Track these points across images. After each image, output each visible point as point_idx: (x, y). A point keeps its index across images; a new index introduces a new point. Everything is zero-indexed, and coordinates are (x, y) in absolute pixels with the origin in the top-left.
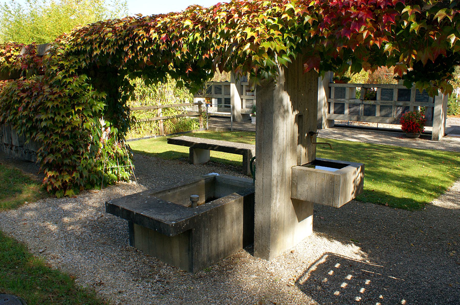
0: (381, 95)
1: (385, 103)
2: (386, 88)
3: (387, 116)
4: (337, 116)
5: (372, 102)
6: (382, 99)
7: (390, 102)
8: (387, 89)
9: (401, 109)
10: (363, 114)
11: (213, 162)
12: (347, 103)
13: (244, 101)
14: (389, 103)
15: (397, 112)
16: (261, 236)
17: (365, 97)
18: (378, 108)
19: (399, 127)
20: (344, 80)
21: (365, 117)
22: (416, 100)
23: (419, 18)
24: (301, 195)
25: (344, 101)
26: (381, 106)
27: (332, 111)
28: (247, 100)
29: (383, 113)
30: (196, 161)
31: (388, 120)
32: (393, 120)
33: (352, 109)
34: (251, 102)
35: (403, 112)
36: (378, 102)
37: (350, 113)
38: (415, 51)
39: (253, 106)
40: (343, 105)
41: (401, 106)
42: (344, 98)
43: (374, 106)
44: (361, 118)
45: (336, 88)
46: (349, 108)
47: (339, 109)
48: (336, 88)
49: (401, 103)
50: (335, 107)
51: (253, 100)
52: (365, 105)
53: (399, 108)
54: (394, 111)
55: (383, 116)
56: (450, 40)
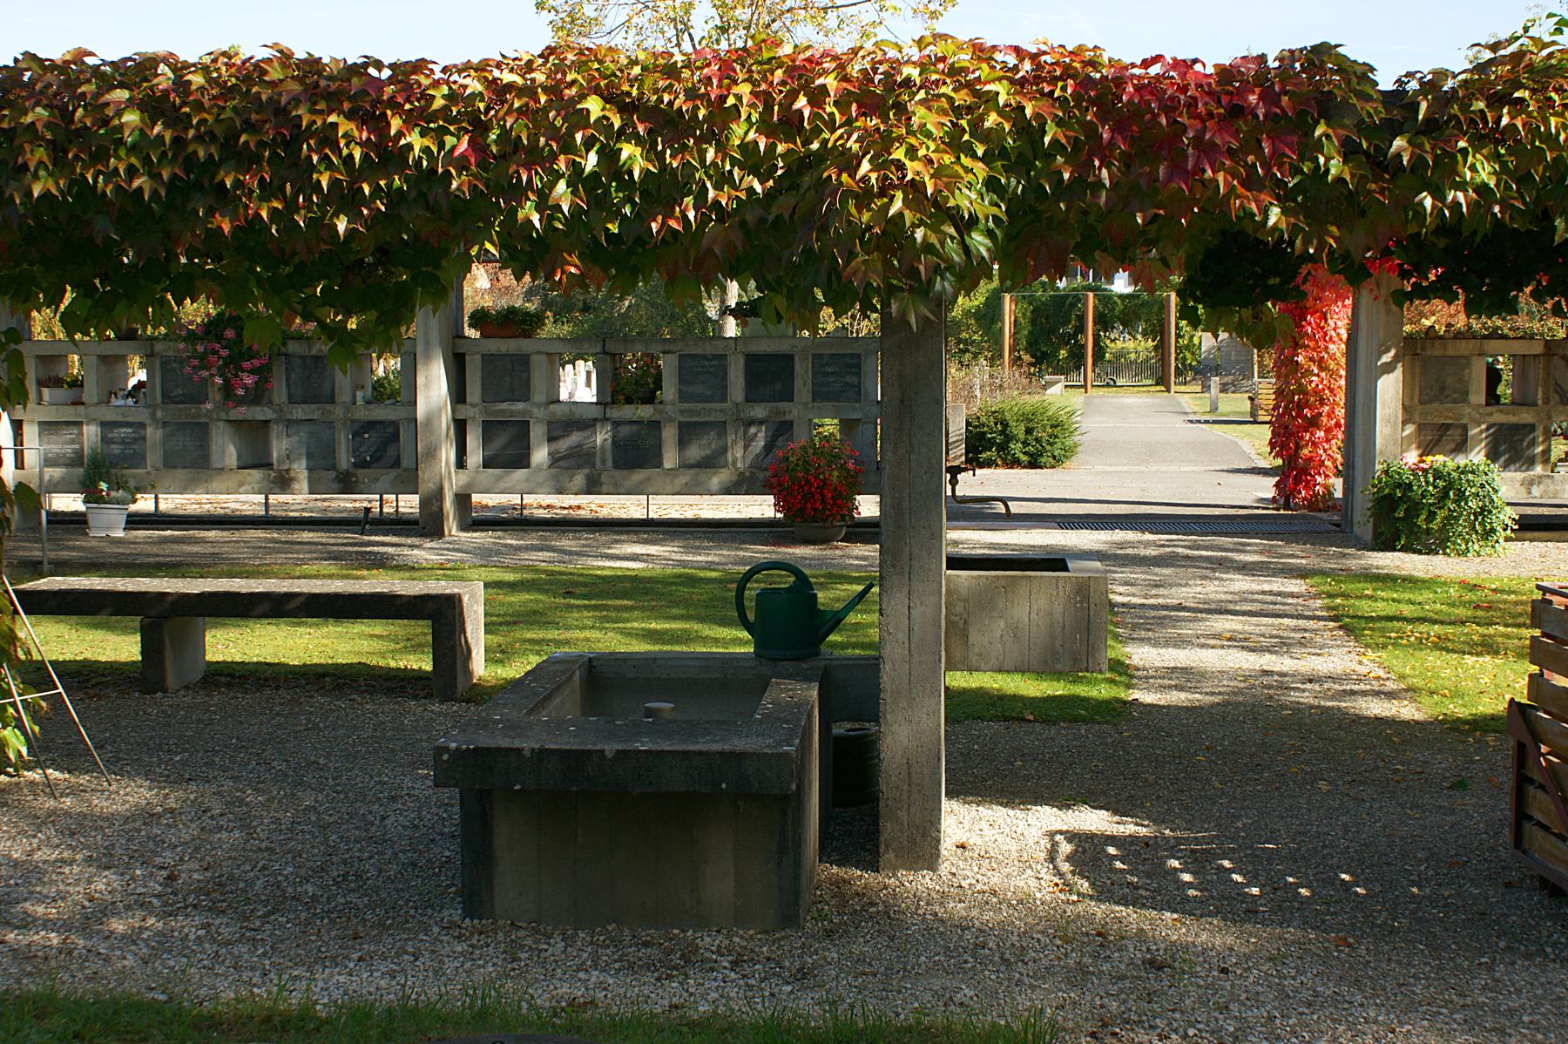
0: (681, 381)
1: (699, 413)
2: (699, 352)
3: (710, 463)
4: (499, 479)
5: (645, 412)
6: (683, 397)
7: (717, 406)
8: (704, 357)
9: (761, 435)
10: (610, 463)
11: (232, 676)
12: (539, 420)
13: (31, 433)
14: (713, 411)
15: (746, 448)
16: (905, 797)
17: (614, 393)
18: (669, 434)
19: (762, 507)
20: (524, 322)
21: (618, 473)
22: (816, 396)
23: (1349, 151)
24: (980, 655)
25: (525, 412)
26: (681, 425)
27: (475, 457)
28: (47, 427)
29: (695, 452)
30: (171, 680)
31: (715, 482)
32: (734, 478)
33: (564, 444)
34: (70, 434)
35: (768, 448)
36: (668, 408)
37: (555, 459)
38: (1333, 229)
39: (79, 454)
40: (524, 427)
41: (761, 422)
42: (526, 398)
43: (655, 426)
44: (604, 478)
45: (488, 359)
46: (551, 440)
47: (505, 448)
48: (488, 359)
49: (759, 411)
50: (486, 440)
51: (79, 424)
52: (616, 424)
53: (753, 430)
54: (734, 442)
55: (691, 466)
56: (1421, 203)
